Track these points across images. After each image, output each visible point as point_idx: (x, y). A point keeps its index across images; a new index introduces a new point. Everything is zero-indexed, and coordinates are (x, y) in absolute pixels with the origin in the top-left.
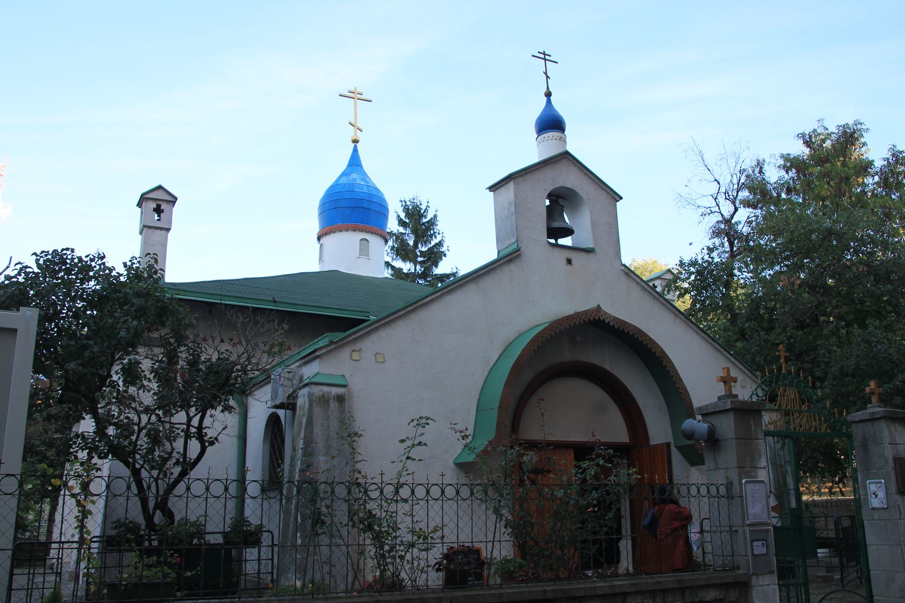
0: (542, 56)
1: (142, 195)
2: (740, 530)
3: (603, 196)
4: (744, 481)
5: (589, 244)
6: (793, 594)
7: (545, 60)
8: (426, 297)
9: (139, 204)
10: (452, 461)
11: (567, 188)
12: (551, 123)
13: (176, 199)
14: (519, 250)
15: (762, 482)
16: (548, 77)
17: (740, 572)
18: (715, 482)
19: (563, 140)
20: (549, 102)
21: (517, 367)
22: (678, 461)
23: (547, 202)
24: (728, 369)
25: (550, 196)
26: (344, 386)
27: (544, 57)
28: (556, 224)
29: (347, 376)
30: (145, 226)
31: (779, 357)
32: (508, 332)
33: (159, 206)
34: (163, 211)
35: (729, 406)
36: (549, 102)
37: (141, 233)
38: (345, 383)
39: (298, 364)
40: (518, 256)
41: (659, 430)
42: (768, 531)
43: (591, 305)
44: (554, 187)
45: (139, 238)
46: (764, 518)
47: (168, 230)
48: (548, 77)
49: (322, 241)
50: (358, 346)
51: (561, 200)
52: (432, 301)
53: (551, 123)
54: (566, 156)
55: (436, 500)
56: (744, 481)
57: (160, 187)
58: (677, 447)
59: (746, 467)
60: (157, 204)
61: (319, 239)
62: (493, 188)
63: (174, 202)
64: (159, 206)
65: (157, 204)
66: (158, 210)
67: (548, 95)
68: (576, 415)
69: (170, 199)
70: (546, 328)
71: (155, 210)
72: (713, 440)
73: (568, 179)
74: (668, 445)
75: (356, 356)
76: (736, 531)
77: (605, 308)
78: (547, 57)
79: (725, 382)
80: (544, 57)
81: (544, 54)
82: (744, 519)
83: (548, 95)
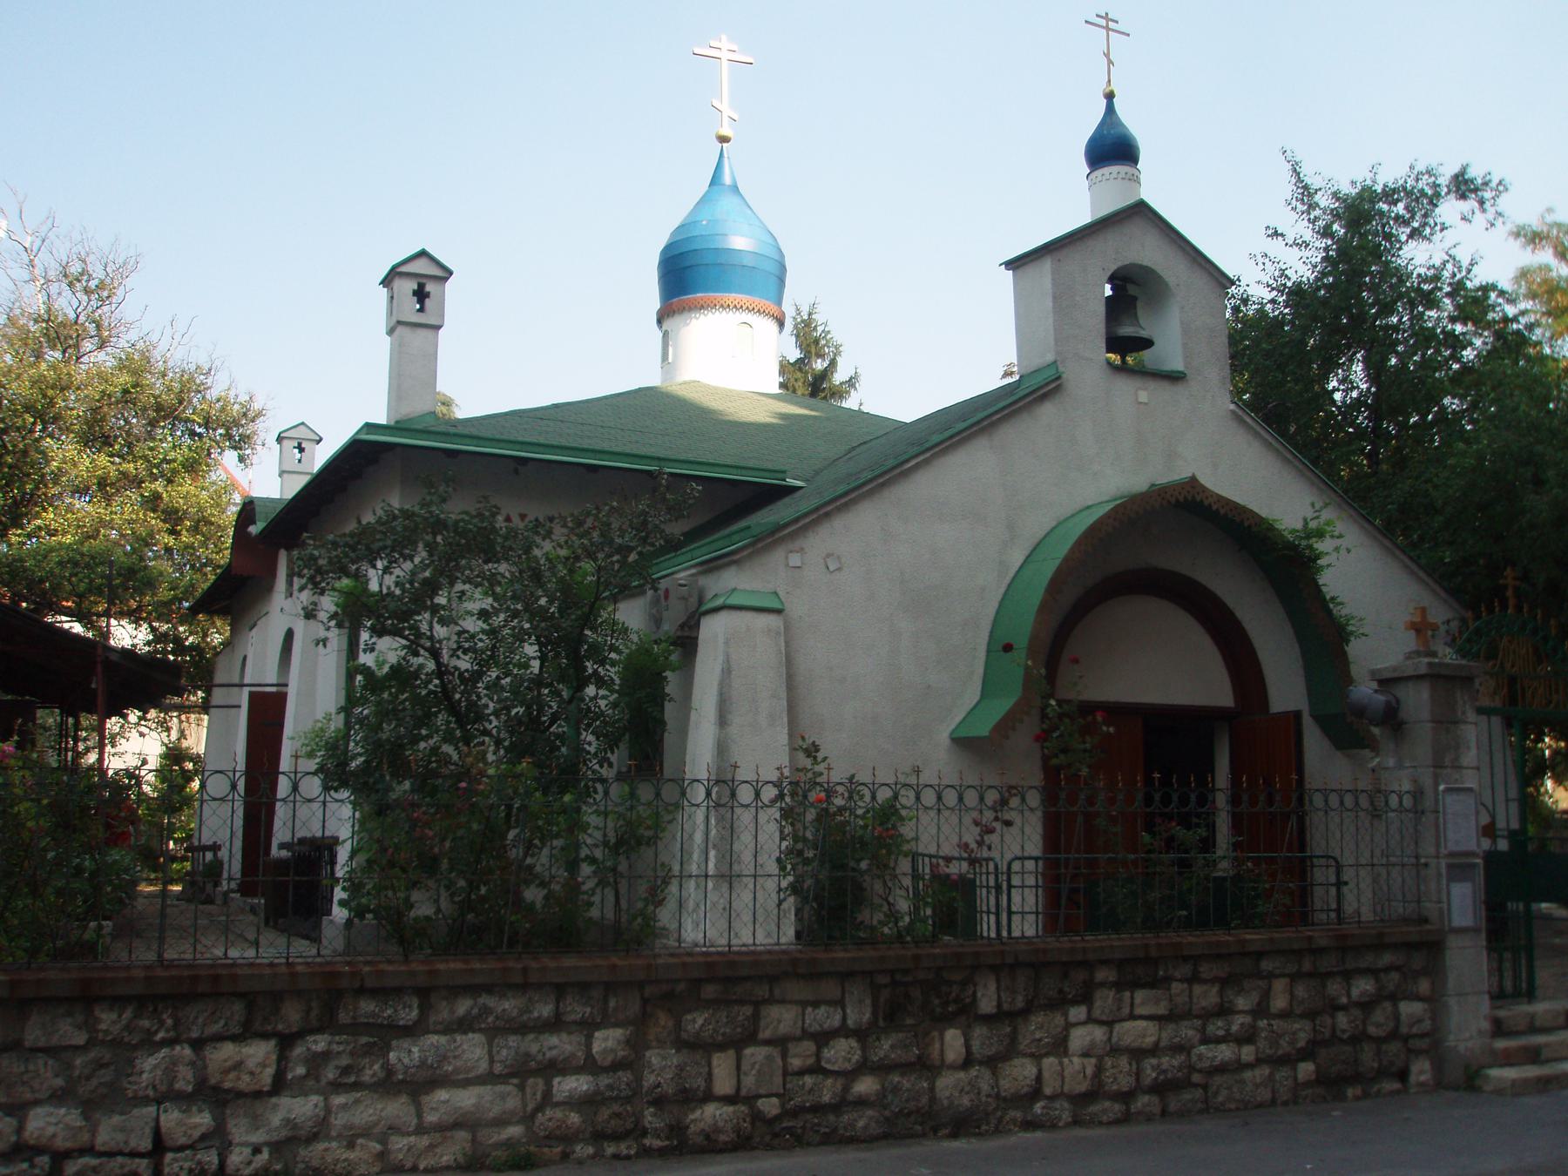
0: (1103, 22)
1: (394, 268)
2: (1433, 862)
3: (1200, 281)
4: (1442, 787)
5: (1177, 364)
6: (1507, 965)
7: (1107, 28)
8: (907, 461)
9: (387, 282)
10: (943, 735)
11: (1141, 267)
12: (1112, 149)
13: (451, 273)
14: (1059, 378)
15: (1470, 790)
16: (1110, 62)
17: (1429, 927)
18: (1396, 788)
19: (1136, 180)
20: (1110, 109)
21: (1056, 584)
22: (1314, 743)
23: (1108, 291)
24: (1423, 610)
25: (1112, 279)
26: (779, 612)
27: (1107, 23)
28: (1126, 330)
29: (781, 594)
30: (399, 323)
31: (1505, 587)
32: (1036, 525)
33: (421, 286)
34: (428, 295)
35: (1423, 670)
36: (1110, 109)
37: (391, 332)
38: (777, 605)
39: (694, 571)
40: (1058, 389)
41: (1286, 688)
42: (1474, 866)
43: (1180, 473)
44: (1120, 264)
45: (386, 342)
46: (1472, 845)
47: (439, 327)
48: (1110, 62)
49: (667, 325)
50: (798, 544)
51: (1131, 292)
52: (917, 467)
53: (1112, 149)
54: (1141, 210)
55: (747, 806)
56: (1442, 787)
57: (423, 254)
58: (1315, 718)
59: (1444, 759)
60: (418, 285)
61: (660, 322)
62: (1014, 264)
63: (446, 279)
64: (421, 286)
65: (418, 285)
66: (421, 295)
67: (1110, 96)
68: (1163, 667)
69: (439, 273)
70: (1108, 516)
71: (415, 293)
72: (1392, 719)
73: (1145, 251)
74: (1297, 715)
75: (795, 560)
76: (1426, 865)
77: (1207, 481)
78: (1111, 25)
79: (1418, 631)
80: (1107, 23)
81: (1106, 17)
82: (1438, 845)
83: (1110, 96)
